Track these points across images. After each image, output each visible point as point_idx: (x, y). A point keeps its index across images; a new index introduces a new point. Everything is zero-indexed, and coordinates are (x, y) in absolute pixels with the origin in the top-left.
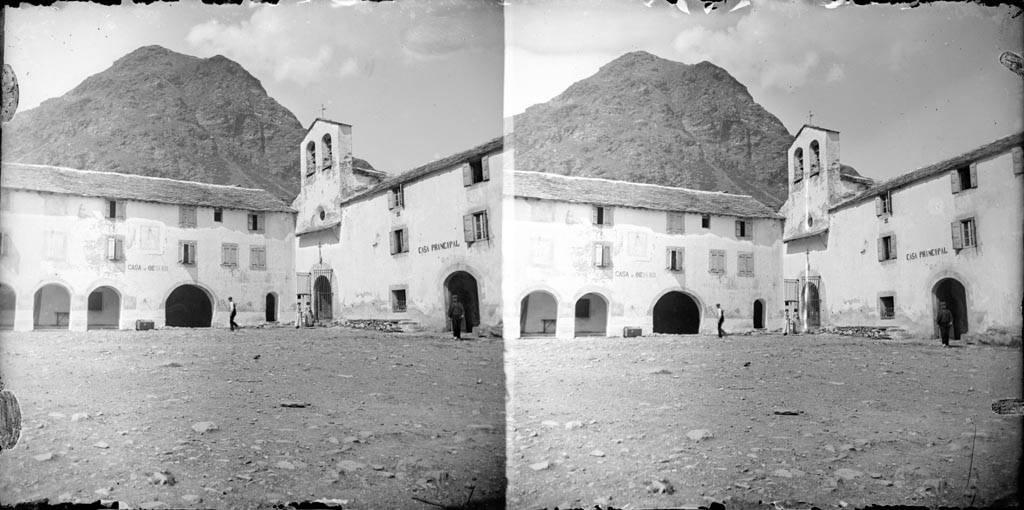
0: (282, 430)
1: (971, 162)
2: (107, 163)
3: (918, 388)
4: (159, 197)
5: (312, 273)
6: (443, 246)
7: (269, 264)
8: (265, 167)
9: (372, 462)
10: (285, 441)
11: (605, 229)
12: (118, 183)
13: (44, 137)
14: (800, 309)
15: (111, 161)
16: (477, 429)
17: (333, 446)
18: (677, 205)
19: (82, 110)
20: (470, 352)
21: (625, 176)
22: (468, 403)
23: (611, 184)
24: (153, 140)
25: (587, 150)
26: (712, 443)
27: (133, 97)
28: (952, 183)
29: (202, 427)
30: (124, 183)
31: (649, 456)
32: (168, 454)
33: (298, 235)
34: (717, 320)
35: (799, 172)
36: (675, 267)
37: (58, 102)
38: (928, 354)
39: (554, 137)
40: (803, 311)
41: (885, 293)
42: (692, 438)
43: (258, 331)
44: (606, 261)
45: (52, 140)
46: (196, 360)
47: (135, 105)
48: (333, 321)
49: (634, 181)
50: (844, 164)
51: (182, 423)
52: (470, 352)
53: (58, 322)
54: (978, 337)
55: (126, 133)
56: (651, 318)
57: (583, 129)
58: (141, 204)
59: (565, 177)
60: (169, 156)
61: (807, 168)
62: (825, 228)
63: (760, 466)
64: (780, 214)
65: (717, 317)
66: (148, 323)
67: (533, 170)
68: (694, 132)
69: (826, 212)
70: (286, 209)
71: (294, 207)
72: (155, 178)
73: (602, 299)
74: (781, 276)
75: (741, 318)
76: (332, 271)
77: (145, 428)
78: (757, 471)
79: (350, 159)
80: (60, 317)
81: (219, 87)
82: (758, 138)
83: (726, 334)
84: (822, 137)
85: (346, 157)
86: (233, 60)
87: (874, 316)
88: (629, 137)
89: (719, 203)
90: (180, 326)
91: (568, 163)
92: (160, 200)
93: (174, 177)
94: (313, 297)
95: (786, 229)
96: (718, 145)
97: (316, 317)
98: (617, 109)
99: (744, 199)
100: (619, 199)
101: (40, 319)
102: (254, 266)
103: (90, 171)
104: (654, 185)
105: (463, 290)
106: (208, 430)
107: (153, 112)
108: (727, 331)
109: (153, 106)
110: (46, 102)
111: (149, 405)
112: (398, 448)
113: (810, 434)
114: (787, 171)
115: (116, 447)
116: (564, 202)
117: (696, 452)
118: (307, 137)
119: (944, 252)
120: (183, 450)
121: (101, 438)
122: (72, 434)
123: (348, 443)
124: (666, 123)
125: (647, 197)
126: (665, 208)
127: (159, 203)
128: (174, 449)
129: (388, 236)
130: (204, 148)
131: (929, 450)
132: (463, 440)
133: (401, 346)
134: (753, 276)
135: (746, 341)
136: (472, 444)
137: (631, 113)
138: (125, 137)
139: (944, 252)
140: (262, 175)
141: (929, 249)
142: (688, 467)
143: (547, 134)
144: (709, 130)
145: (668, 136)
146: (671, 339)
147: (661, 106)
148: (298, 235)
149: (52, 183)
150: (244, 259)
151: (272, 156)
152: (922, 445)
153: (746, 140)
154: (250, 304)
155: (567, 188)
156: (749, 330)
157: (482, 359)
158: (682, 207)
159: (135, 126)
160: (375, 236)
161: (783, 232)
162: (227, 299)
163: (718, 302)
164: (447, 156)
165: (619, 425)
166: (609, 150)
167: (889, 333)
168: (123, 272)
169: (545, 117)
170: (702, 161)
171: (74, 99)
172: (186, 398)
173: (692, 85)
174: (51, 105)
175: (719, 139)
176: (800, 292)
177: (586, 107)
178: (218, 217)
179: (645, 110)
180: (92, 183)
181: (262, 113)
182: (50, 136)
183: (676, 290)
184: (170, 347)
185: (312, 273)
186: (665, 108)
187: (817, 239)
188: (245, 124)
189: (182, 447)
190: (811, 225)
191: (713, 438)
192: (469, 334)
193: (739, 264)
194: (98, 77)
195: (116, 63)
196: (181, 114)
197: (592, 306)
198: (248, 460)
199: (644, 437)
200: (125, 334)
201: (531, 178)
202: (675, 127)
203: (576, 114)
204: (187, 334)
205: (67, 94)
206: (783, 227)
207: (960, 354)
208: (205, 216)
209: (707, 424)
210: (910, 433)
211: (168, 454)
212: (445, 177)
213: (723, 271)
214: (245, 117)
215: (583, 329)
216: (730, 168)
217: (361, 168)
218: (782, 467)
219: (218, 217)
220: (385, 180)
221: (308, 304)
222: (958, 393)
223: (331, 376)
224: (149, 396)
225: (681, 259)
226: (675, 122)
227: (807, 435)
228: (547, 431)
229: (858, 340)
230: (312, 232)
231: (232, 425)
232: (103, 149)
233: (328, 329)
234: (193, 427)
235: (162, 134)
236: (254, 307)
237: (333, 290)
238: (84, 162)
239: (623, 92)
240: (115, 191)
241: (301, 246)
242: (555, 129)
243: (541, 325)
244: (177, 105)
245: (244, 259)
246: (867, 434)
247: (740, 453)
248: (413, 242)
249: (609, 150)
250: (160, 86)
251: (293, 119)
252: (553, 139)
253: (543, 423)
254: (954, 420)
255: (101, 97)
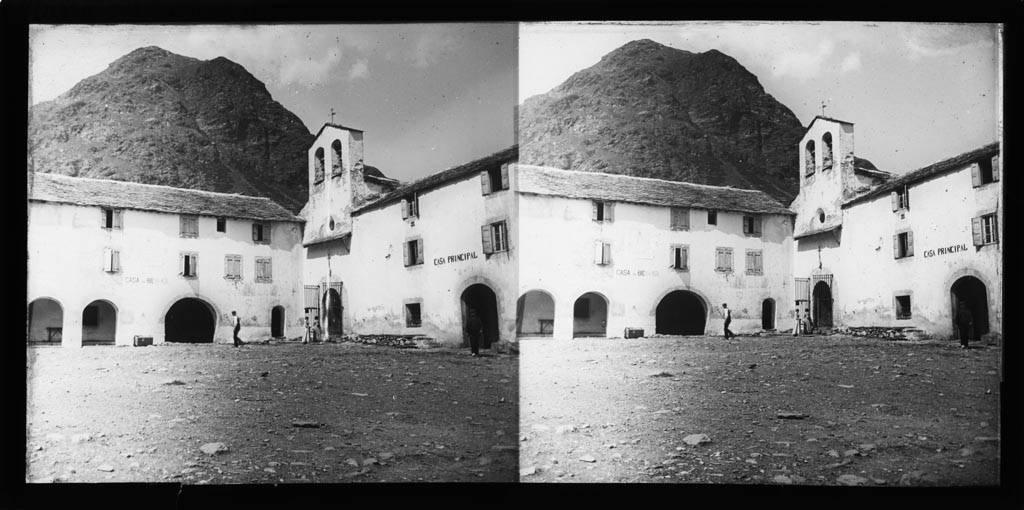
0: (296, 451)
1: (503, 162)
2: (595, 163)
3: (446, 399)
4: (649, 199)
5: (812, 278)
6: (950, 250)
7: (765, 270)
8: (270, 174)
9: (874, 476)
10: (301, 463)
11: (114, 232)
12: (115, 192)
13: (529, 136)
14: (321, 317)
15: (106, 169)
16: (986, 441)
17: (833, 460)
18: (190, 207)
19: (568, 106)
20: (978, 360)
21: (136, 178)
22: (976, 414)
23: (612, 179)
24: (151, 145)
25: (95, 150)
26: (228, 457)
27: (622, 94)
28: (973, 177)
29: (694, 439)
30: (613, 184)
31: (160, 470)
32: (658, 468)
33: (796, 239)
34: (233, 329)
35: (811, 165)
36: (188, 272)
37: (50, 106)
38: (458, 363)
39: (61, 136)
40: (324, 319)
41: (901, 292)
42: (205, 452)
43: (264, 347)
44: (115, 267)
45: (536, 139)
46: (688, 370)
47: (624, 102)
48: (344, 337)
49: (145, 183)
50: (859, 157)
51: (189, 444)
52: (978, 360)
53: (542, 329)
54: (509, 345)
55: (615, 131)
56: (163, 325)
57: (91, 128)
58: (140, 213)
59: (71, 178)
60: (168, 162)
61: (328, 169)
62: (347, 231)
63: (759, 473)
64: (299, 217)
65: (232, 325)
66: (636, 331)
67: (532, 163)
68: (702, 124)
69: (839, 208)
70: (782, 209)
71: (791, 209)
72: (644, 179)
73: (204, 306)
74: (301, 283)
75: (259, 326)
76: (342, 283)
77: (634, 441)
78: (755, 477)
79: (852, 159)
80: (544, 325)
81: (221, 91)
82: (770, 130)
83: (243, 344)
84: (344, 137)
85: (357, 164)
86: (235, 61)
87: (399, 324)
88: (140, 135)
89: (235, 205)
90: (180, 342)
91: (568, 156)
92: (160, 209)
93: (666, 177)
94: (812, 303)
95: (306, 232)
96: (726, 138)
97: (814, 325)
98: (127, 107)
99: (262, 201)
100: (620, 194)
101: (523, 326)
102: (750, 271)
103: (576, 172)
104: (167, 187)
105: (479, 301)
106: (700, 443)
107: (643, 109)
108: (243, 340)
109: (151, 110)
110: (531, 99)
111: (638, 417)
112: (901, 462)
113: (331, 448)
114: (308, 173)
115: (122, 470)
116: (71, 204)
117: (210, 466)
118: (806, 135)
119: (964, 249)
120: (674, 464)
121: (587, 452)
122: (556, 447)
123: (849, 457)
124: (179, 122)
125: (650, 193)
126: (178, 211)
127: (158, 212)
128: (183, 472)
129: (402, 246)
130: (205, 155)
131: (939, 454)
132: (971, 453)
133: (416, 363)
134: (762, 274)
135: (264, 351)
136: (980, 458)
137: (634, 104)
138: (614, 136)
139: (964, 249)
140: (758, 176)
141: (949, 246)
142: (683, 473)
143: (52, 133)
144: (224, 129)
145: (182, 135)
146: (675, 341)
147: (666, 97)
148: (796, 239)
149: (44, 191)
150: (740, 263)
151: (769, 155)
152: (933, 450)
153: (264, 140)
154: (745, 311)
155: (74, 189)
156: (757, 331)
157: (991, 368)
158: (686, 203)
159: (623, 124)
160: (388, 247)
161: (303, 236)
162: (720, 306)
163: (234, 310)
164: (954, 157)
165: (129, 438)
166: (120, 150)
167: (415, 342)
168: (611, 277)
169: (50, 116)
170: (710, 154)
171: (560, 96)
172: (677, 409)
173: (206, 82)
174: (543, 100)
175: (728, 131)
176: (321, 299)
177: (95, 105)
178: (712, 221)
179: (156, 108)
180: (578, 183)
181: (760, 111)
182: (534, 134)
183: (680, 289)
184: (661, 356)
185: (812, 278)
186: (179, 106)
187: (339, 244)
188: (741, 123)
189: (191, 470)
190: (332, 229)
191: (711, 443)
192: (978, 342)
193: (257, 270)
194: (94, 79)
195: (604, 59)
196: (181, 119)
197: (101, 313)
198: (743, 474)
199: (155, 450)
200: (613, 343)
201: (528, 173)
202: (188, 126)
203: (577, 105)
204: (678, 342)
205: (552, 90)
206: (303, 231)
207: (979, 355)
208: (208, 226)
209: (705, 428)
210: (920, 438)
211: (658, 468)
212: (953, 177)
213: (730, 269)
214: (741, 114)
215: (91, 337)
216: (246, 168)
217: (862, 168)
218: (782, 473)
219: (221, 228)
220: (889, 181)
221: (807, 310)
222: (488, 405)
223: (344, 395)
224: (639, 407)
225: (686, 257)
226: (188, 121)
227: (328, 448)
228: (52, 444)
229: (873, 341)
230: (825, 233)
231: (725, 438)
232: (590, 148)
233: (338, 345)
234: (685, 440)
235: (653, 133)
236: (260, 321)
237: (834, 297)
238: (77, 170)
239: (133, 89)
240: (603, 192)
241: (309, 257)
242: (62, 128)
243: (46, 333)
244: (176, 110)
245: (740, 263)
246: (874, 439)
247: (257, 468)
248: (918, 246)
249: (120, 150)
250: (159, 89)
251: (789, 116)
252: (60, 138)
253: (48, 436)
254: (968, 424)
255: (95, 99)
